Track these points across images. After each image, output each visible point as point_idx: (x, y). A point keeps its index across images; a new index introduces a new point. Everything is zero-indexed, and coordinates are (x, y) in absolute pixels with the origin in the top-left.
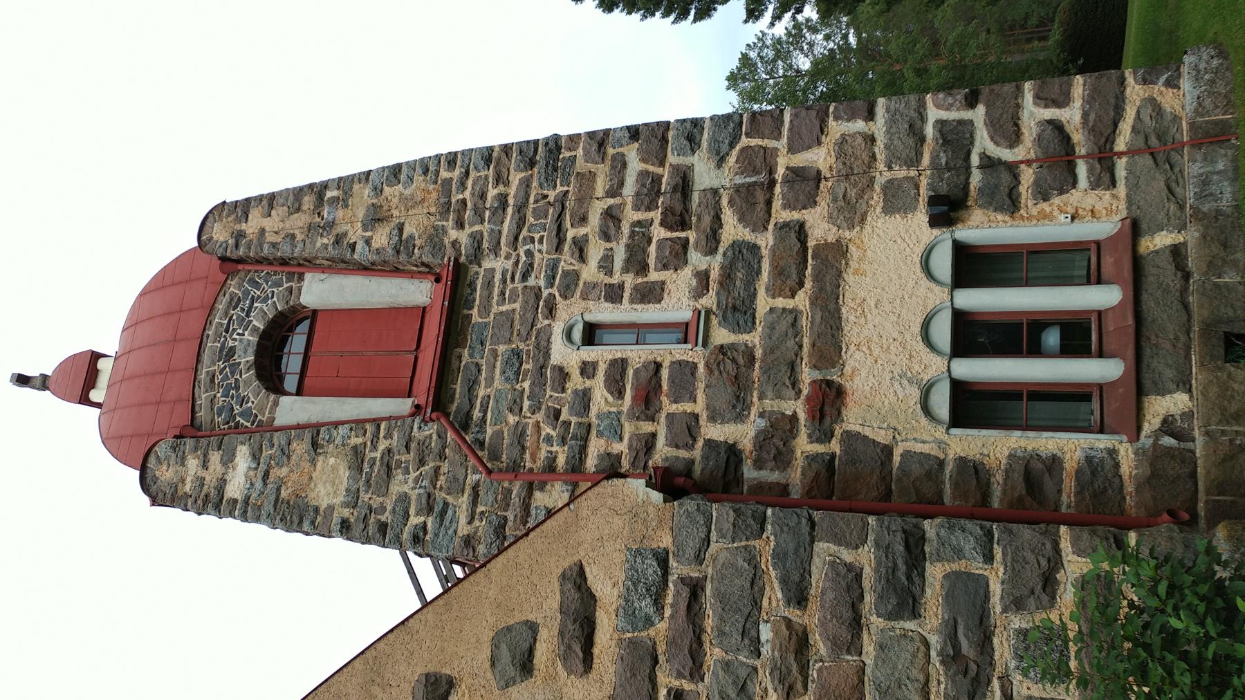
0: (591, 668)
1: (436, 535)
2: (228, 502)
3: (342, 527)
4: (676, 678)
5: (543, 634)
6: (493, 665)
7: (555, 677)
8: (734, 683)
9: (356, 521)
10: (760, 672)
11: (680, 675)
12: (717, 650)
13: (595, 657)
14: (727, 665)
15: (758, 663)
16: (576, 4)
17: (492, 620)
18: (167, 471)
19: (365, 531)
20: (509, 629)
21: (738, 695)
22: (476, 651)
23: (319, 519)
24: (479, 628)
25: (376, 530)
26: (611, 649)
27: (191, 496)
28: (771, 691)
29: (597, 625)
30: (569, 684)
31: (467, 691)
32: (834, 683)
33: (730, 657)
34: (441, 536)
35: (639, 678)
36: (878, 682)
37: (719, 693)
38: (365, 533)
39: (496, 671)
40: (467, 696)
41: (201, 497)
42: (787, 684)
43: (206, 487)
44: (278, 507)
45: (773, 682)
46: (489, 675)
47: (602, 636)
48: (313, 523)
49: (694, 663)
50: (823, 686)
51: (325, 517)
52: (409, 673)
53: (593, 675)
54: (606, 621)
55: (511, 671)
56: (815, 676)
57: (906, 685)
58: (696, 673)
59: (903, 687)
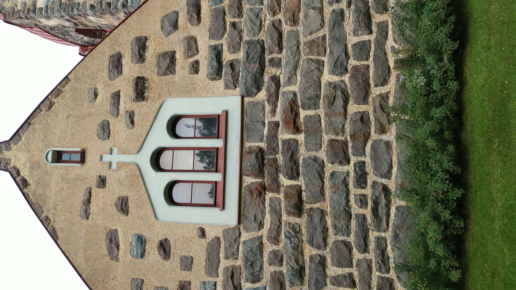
0: (200, 22)
1: (132, 3)
2: (39, 9)
3: (91, 7)
4: (233, 18)
5: (181, 14)
6: (162, 29)
7: (187, 28)
8: (254, 14)
9: (97, 4)
10: (264, 9)
11: (234, 17)
12: (247, 5)
13: (201, 17)
14: (251, 10)
15: (262, 7)
16: (209, 193)
17: (160, 14)
18: (8, 3)
19: (102, 7)
20: (167, 15)
21: (256, 18)
22: (155, 26)
23: (80, 7)
24: (155, 17)
25: (106, 5)
26: (208, 14)
27: (21, 11)
28: (267, 15)
29: (202, 7)
30: (193, 29)
31: (153, 40)
32: (290, 7)
33: (253, 6)
34: (134, 3)
35: (219, 20)
36: (305, 3)
37: (249, 19)
38: (102, 8)
39: (164, 31)
40: (153, 41)
41: (26, 10)
42: (273, 11)
43: (27, 6)
44: (61, 6)
45: (268, 11)
46: (161, 33)
47: (204, 10)
48: (78, 9)
49: (239, 11)
50: (286, 8)
51: (83, 6)
52: (129, 38)
53: (202, 24)
54: (205, 5)
55: (170, 29)
56: (283, 6)
57: (315, 2)
58: (240, 15)
59: (314, 3)
